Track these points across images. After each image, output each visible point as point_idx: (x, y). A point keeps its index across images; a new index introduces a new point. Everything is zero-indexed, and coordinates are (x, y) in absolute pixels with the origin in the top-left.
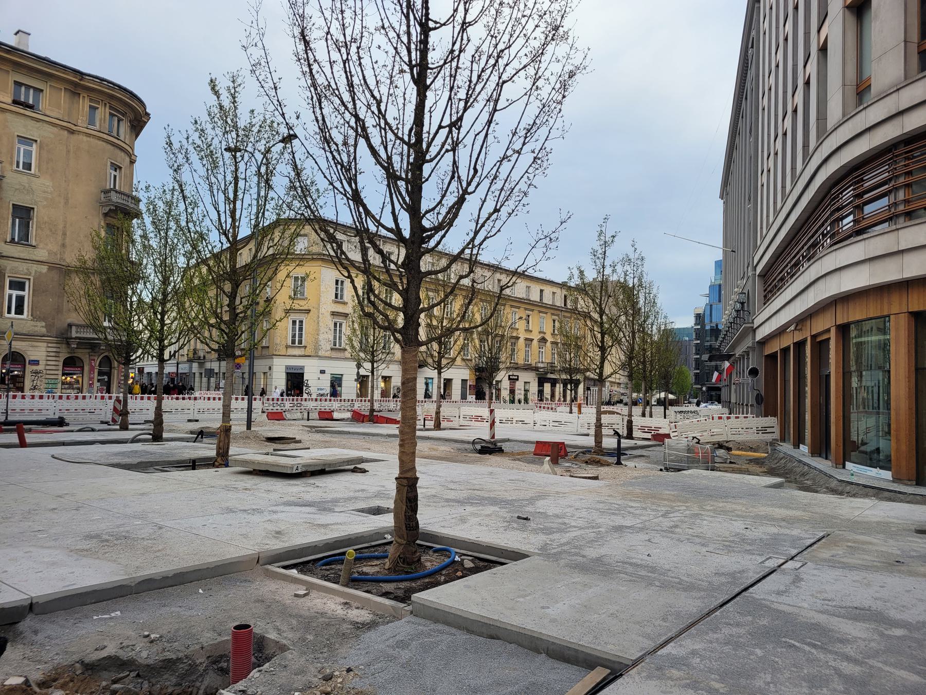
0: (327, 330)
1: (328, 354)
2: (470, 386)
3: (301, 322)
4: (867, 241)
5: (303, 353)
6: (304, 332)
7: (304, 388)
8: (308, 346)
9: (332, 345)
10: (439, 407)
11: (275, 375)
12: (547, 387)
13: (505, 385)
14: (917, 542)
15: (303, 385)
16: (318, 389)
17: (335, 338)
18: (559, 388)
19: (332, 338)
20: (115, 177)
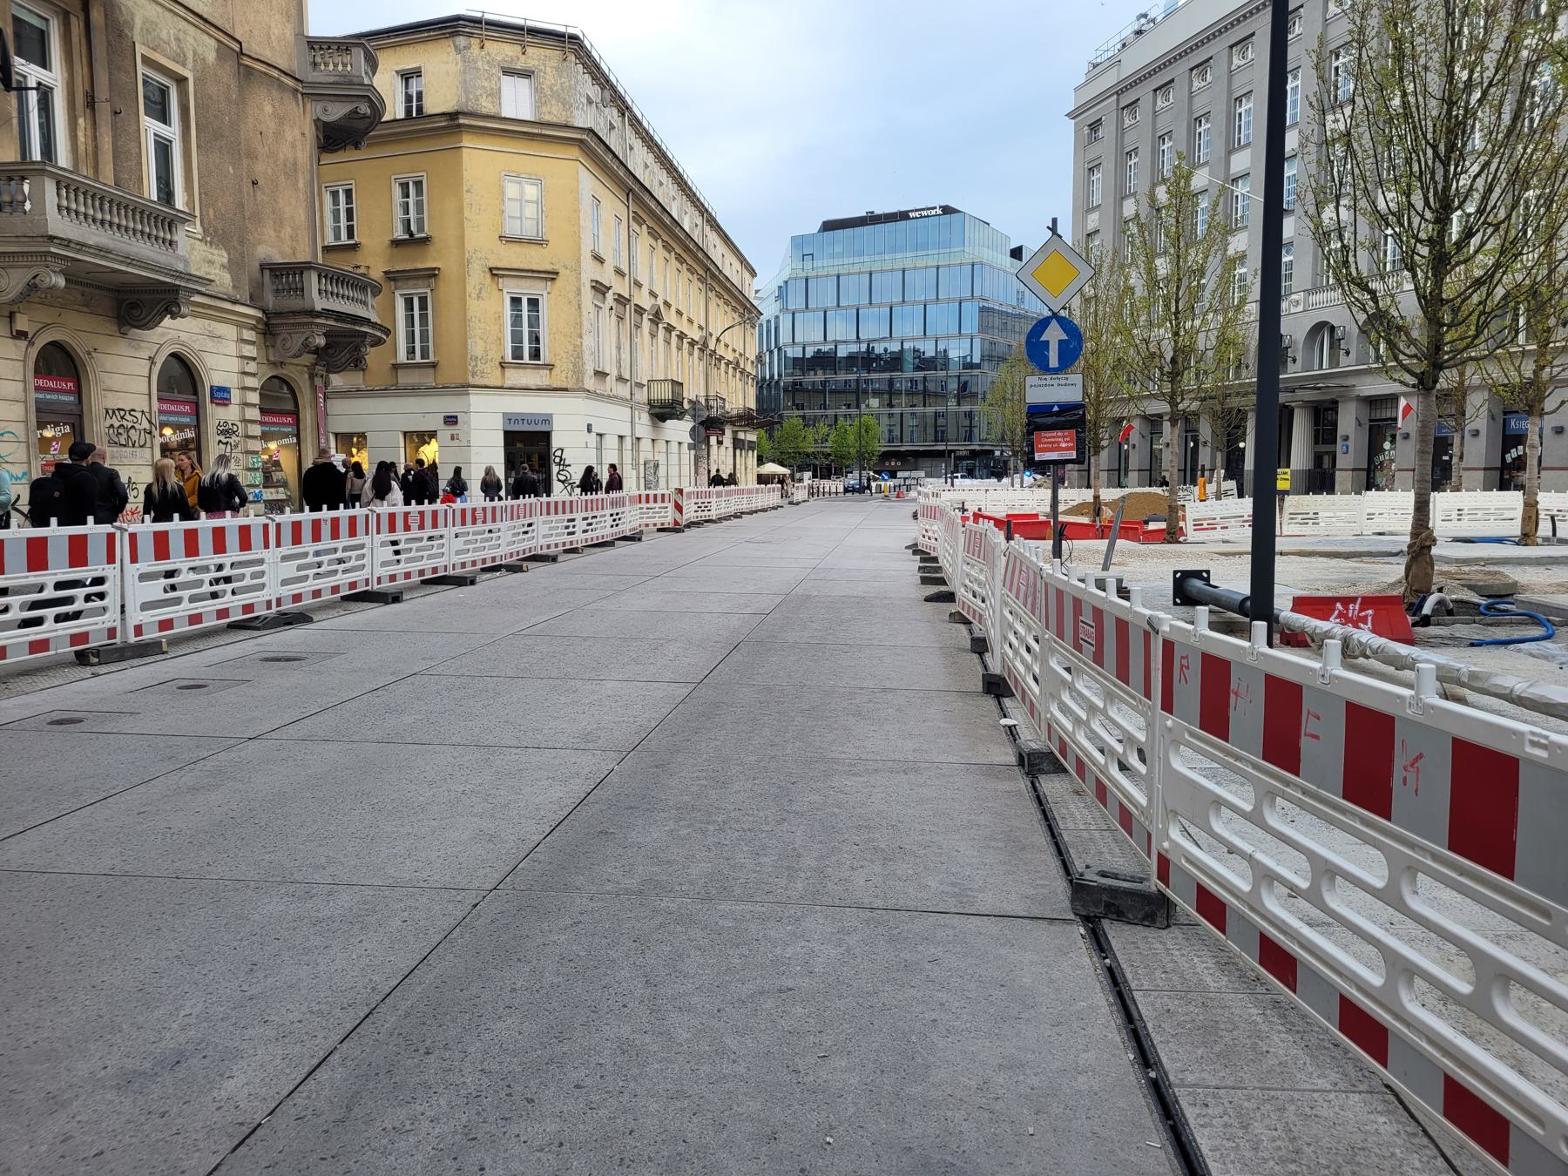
3: (534, 303)
5: (545, 382)
7: (555, 469)
8: (557, 363)
10: (1422, 508)
14: (1093, 737)
20: (163, 149)
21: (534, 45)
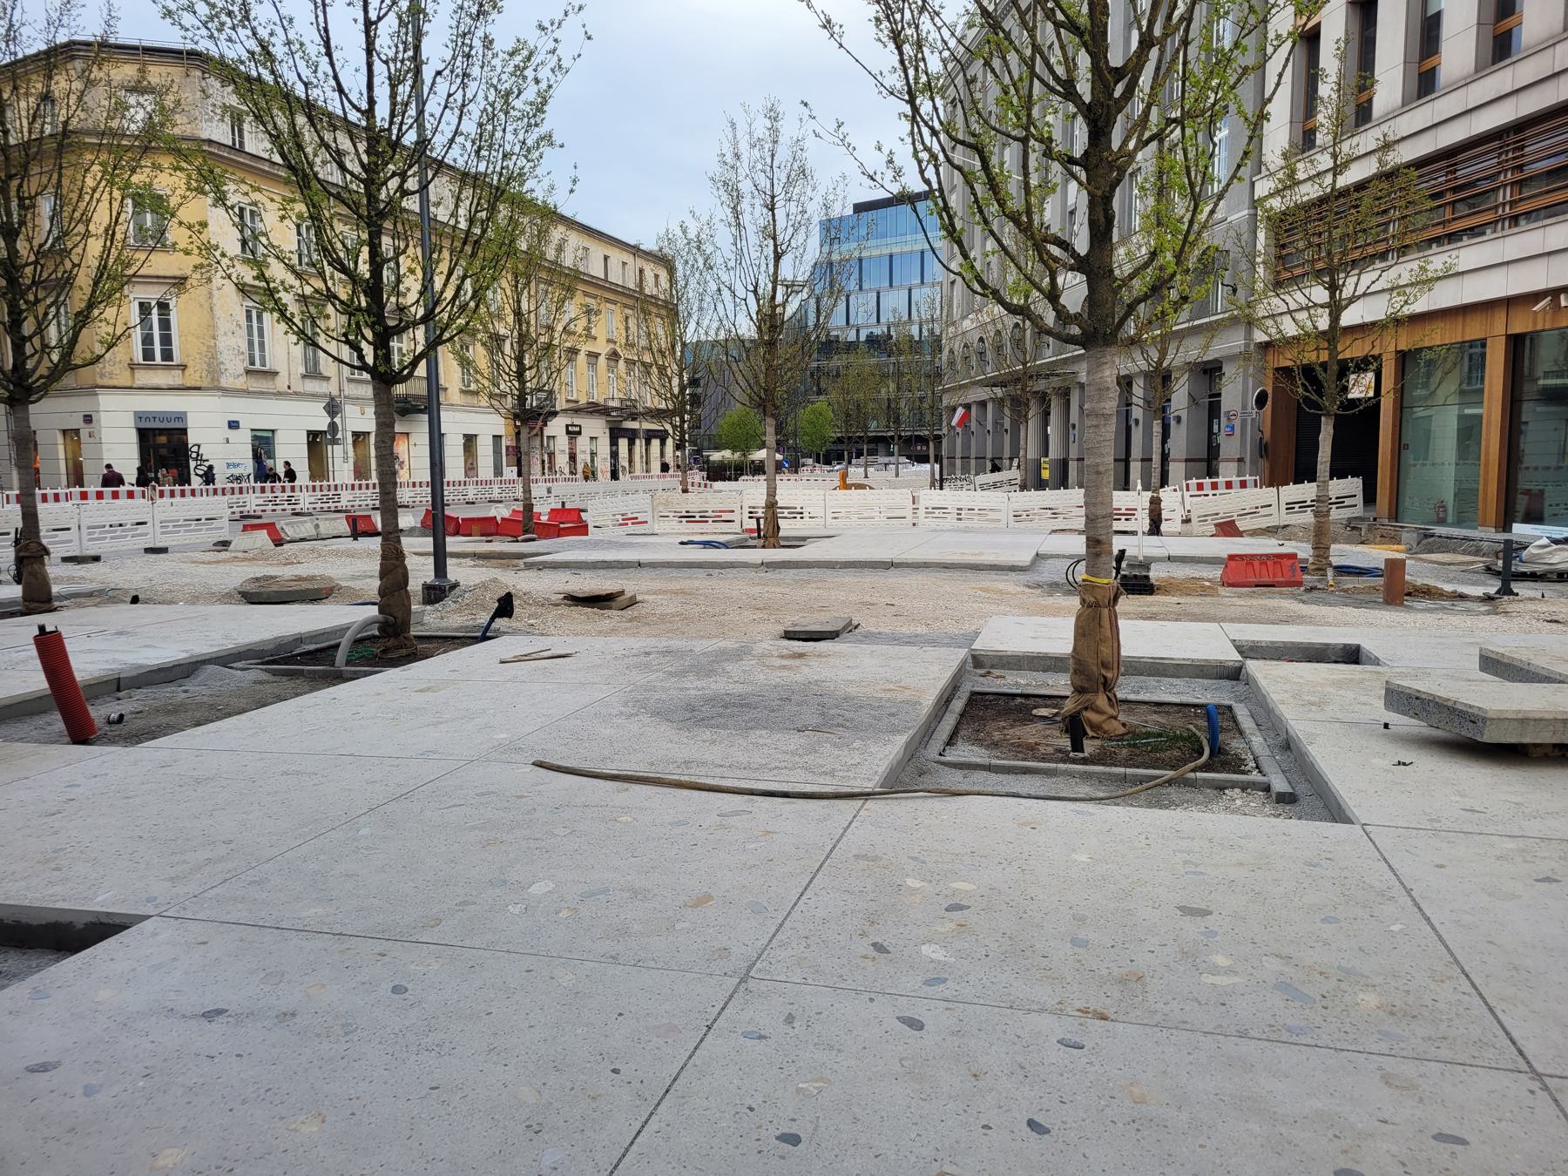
0: (234, 327)
1: (241, 382)
2: (507, 447)
4: (1552, 258)
6: (174, 332)
7: (192, 464)
8: (190, 364)
9: (247, 363)
11: (107, 435)
12: (623, 443)
13: (562, 443)
15: (187, 457)
16: (228, 465)
17: (251, 343)
18: (639, 445)
19: (244, 346)
21: (154, 63)
